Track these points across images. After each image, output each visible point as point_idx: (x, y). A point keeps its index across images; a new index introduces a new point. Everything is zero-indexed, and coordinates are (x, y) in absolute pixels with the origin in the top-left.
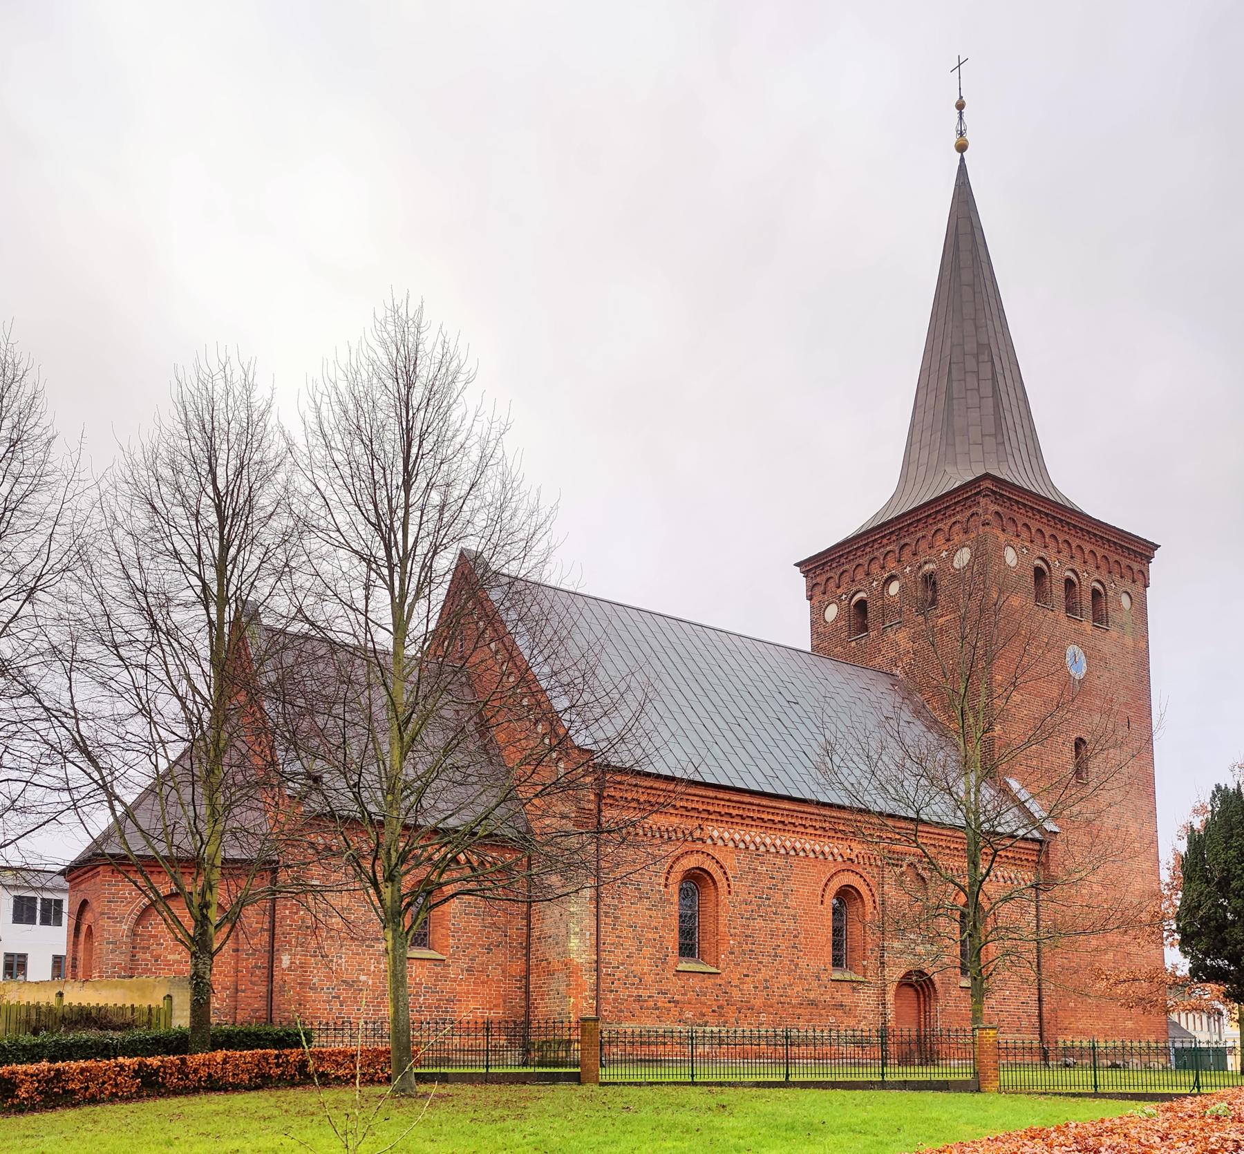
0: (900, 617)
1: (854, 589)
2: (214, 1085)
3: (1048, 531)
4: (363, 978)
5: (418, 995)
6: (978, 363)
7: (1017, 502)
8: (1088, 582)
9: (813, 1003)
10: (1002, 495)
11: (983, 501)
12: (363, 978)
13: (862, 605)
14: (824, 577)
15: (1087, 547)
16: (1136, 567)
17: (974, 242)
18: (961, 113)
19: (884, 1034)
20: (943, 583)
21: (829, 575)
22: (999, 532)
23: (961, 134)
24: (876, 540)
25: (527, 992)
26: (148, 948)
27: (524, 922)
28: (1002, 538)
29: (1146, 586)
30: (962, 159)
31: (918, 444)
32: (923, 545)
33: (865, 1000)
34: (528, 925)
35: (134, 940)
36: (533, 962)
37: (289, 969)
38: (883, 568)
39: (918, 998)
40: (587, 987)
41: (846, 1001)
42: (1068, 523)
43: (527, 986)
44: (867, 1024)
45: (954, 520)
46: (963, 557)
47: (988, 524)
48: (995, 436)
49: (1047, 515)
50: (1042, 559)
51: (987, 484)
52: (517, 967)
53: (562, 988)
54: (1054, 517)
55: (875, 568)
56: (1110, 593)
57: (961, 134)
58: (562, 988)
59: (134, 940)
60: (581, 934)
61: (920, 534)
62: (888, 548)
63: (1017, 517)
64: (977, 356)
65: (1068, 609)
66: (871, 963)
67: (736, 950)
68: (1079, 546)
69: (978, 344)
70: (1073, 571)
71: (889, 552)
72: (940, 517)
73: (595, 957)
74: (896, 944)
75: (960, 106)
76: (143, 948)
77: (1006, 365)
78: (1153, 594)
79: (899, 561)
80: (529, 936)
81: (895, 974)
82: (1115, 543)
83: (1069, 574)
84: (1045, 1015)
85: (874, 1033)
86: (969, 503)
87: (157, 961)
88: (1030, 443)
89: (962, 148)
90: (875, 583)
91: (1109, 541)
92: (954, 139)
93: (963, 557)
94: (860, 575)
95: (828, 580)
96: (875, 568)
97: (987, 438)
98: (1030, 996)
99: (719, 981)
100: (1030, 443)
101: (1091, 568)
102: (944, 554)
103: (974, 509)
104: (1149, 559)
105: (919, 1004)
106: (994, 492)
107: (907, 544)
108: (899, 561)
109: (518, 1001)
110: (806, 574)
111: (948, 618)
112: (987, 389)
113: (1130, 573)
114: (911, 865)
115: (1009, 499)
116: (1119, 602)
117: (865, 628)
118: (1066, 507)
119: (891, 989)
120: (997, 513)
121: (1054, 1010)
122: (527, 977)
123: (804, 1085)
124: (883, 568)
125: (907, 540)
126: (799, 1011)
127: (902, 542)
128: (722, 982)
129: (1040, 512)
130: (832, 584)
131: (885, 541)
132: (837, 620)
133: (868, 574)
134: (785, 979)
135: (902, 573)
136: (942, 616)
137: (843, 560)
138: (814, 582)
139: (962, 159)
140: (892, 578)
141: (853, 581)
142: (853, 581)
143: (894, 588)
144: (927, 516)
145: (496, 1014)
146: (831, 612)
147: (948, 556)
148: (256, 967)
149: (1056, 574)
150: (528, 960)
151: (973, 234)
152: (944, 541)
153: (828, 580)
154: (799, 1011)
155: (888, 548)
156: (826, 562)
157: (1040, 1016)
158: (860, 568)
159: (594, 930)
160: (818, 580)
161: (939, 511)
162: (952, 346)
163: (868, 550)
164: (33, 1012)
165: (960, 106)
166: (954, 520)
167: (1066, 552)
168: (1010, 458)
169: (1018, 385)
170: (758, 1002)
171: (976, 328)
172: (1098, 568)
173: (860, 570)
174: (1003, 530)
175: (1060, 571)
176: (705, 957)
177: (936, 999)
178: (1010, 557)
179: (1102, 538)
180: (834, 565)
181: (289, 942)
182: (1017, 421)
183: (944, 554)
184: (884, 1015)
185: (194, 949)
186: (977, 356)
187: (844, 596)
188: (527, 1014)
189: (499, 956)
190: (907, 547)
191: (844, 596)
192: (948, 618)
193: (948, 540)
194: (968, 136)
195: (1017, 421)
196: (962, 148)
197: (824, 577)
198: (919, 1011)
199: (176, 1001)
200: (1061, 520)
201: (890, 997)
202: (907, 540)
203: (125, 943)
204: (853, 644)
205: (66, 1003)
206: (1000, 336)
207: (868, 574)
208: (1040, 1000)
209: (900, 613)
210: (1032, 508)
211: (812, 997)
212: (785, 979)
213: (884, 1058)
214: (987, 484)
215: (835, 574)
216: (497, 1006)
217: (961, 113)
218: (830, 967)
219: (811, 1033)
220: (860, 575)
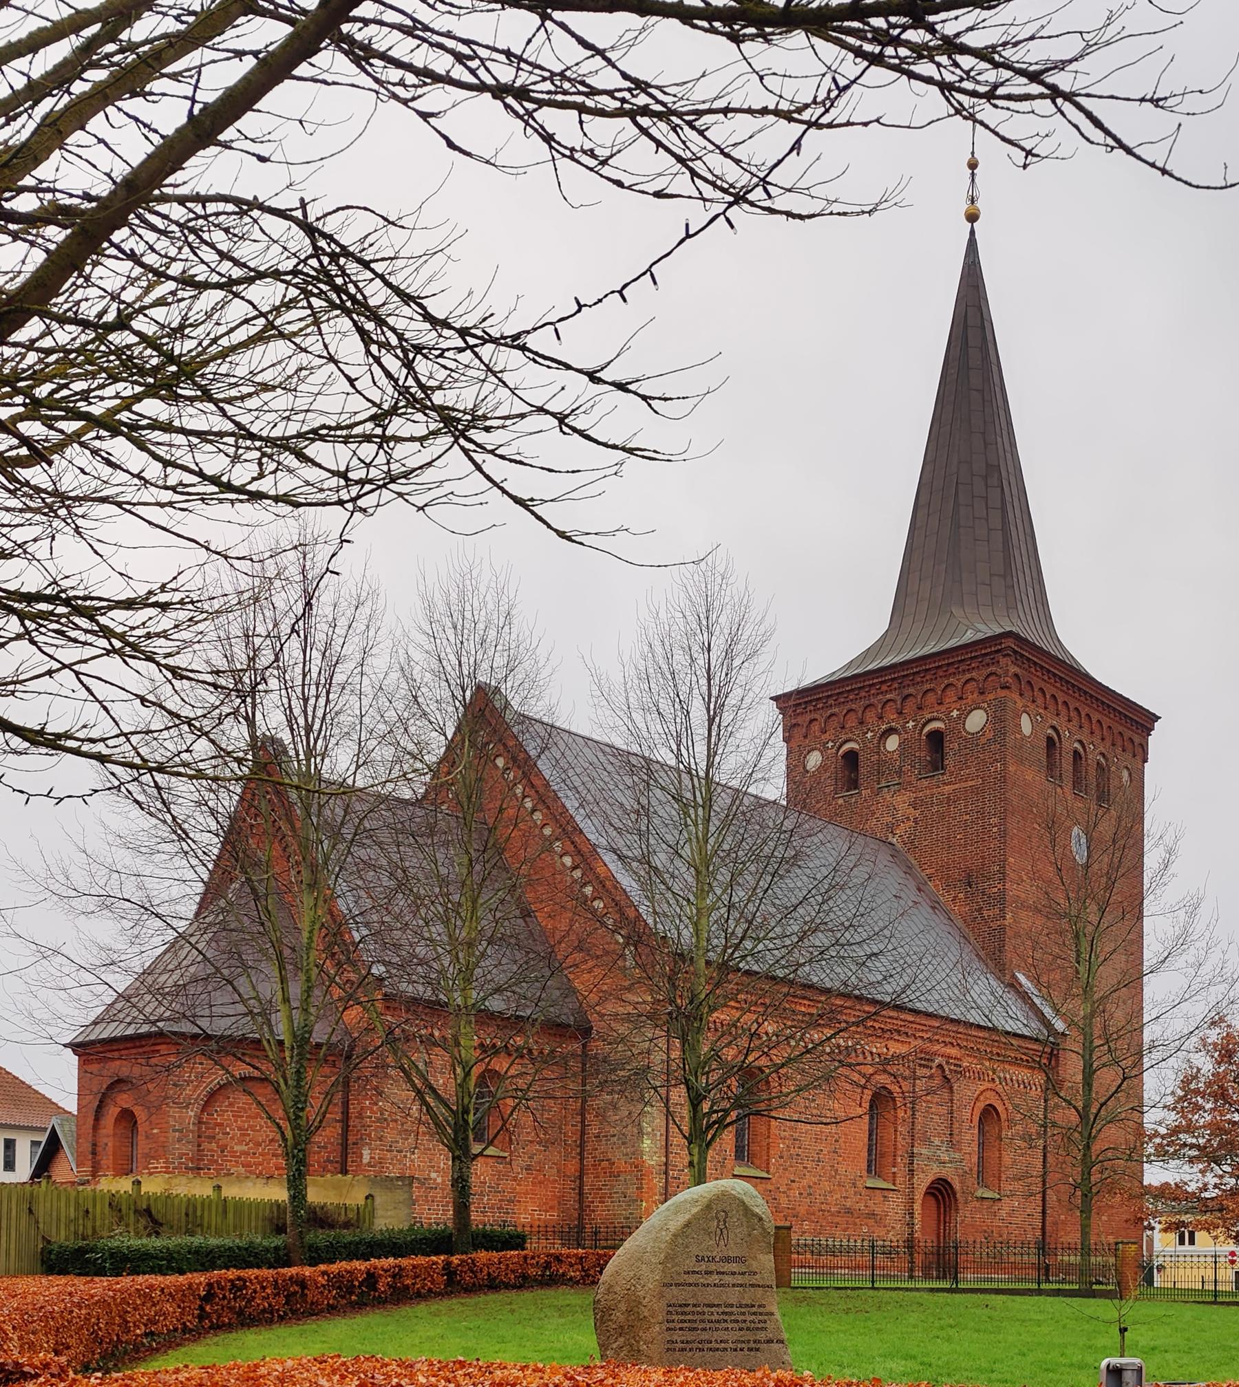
0: (900, 777)
1: (844, 737)
2: (493, 1285)
3: (1061, 698)
4: (433, 1175)
5: (482, 1194)
6: (986, 485)
7: (1035, 663)
8: (1093, 756)
9: (849, 1211)
10: (1022, 656)
11: (1003, 661)
12: (433, 1175)
13: (852, 757)
14: (808, 717)
15: (1095, 717)
16: (1137, 739)
17: (984, 338)
18: (973, 174)
19: (910, 1244)
20: (951, 746)
21: (813, 716)
22: (1016, 696)
23: (973, 202)
24: (873, 684)
25: (581, 1194)
26: (214, 1137)
27: (579, 1118)
28: (1020, 704)
29: (1145, 760)
30: (972, 232)
31: (918, 574)
32: (931, 698)
33: (894, 1207)
34: (583, 1122)
35: (199, 1129)
36: (589, 1161)
37: (369, 1164)
38: (881, 718)
39: (939, 1208)
40: (657, 1191)
41: (878, 1210)
42: (1080, 689)
43: (581, 1188)
44: (894, 1235)
45: (968, 676)
46: (976, 721)
47: (1008, 688)
48: (1004, 577)
49: (1061, 678)
50: (1054, 728)
51: (1010, 643)
52: (572, 1167)
53: (631, 1191)
54: (1067, 682)
55: (871, 716)
56: (1113, 769)
57: (973, 202)
58: (631, 1191)
59: (199, 1129)
60: (652, 1135)
61: (927, 686)
62: (888, 696)
63: (1034, 680)
64: (986, 478)
65: (1099, 799)
66: (901, 1170)
67: (785, 1154)
68: (1099, 721)
69: (987, 465)
70: (1080, 742)
71: (889, 701)
72: (952, 670)
73: (664, 1159)
74: (924, 1151)
75: (973, 165)
76: (209, 1137)
77: (1015, 491)
78: (1151, 771)
79: (901, 713)
80: (583, 1133)
81: (923, 1182)
82: (1120, 713)
83: (1076, 745)
84: (1048, 1228)
85: (901, 1243)
86: (987, 660)
87: (222, 1151)
88: (1037, 587)
89: (972, 217)
90: (869, 735)
91: (1114, 709)
92: (964, 206)
93: (976, 721)
94: (852, 722)
95: (811, 721)
96: (871, 716)
97: (996, 578)
98: (1035, 1207)
99: (770, 1187)
100: (1037, 587)
101: (1097, 740)
102: (955, 713)
103: (993, 669)
104: (1149, 730)
105: (939, 1214)
106: (1015, 652)
107: (910, 695)
108: (901, 713)
109: (572, 1203)
110: (782, 710)
111: (956, 786)
112: (996, 521)
113: (1131, 746)
114: (940, 1066)
115: (1028, 659)
116: (1121, 778)
117: (854, 784)
118: (1072, 666)
119: (919, 1196)
120: (1016, 675)
121: (1056, 1223)
122: (581, 1178)
123: (1222, 1303)
124: (881, 718)
125: (911, 690)
126: (837, 1220)
127: (906, 692)
128: (771, 1188)
129: (1055, 675)
130: (815, 727)
131: (884, 688)
132: (822, 768)
133: (861, 723)
134: (826, 1185)
135: (904, 727)
136: (950, 784)
137: (831, 702)
138: (794, 721)
139: (972, 232)
140: (891, 731)
141: (843, 728)
142: (843, 728)
143: (892, 743)
144: (937, 668)
145: (552, 1216)
146: (814, 760)
147: (959, 717)
148: (328, 1161)
149: (1065, 744)
150: (582, 1160)
151: (984, 328)
152: (955, 699)
153: (811, 721)
154: (837, 1220)
155: (888, 696)
156: (811, 701)
157: (1043, 1229)
158: (851, 714)
159: (663, 1130)
160: (800, 720)
161: (952, 663)
162: (960, 462)
163: (863, 694)
164: (275, 1209)
165: (973, 165)
166: (968, 676)
167: (1040, 701)
168: (1019, 606)
169: (1026, 517)
170: (802, 1210)
171: (986, 445)
172: (1103, 739)
173: (852, 715)
174: (1021, 695)
175: (1069, 744)
176: (755, 1161)
177: (957, 1210)
178: (1026, 725)
179: (1109, 706)
180: (820, 706)
181: (369, 1135)
182: (1025, 560)
183: (955, 713)
184: (911, 1225)
185: (457, 1153)
186: (986, 478)
187: (830, 744)
188: (580, 1218)
189: (555, 1154)
190: (911, 698)
191: (830, 744)
192: (956, 786)
193: (961, 698)
194: (979, 204)
195: (1025, 560)
196: (972, 217)
197: (808, 717)
198: (939, 1221)
199: (378, 1200)
200: (1073, 686)
201: (917, 1207)
202: (911, 690)
203: (192, 1132)
204: (841, 801)
205: (143, 1190)
206: (1009, 455)
207: (861, 723)
208: (1044, 1212)
209: (900, 773)
210: (1049, 671)
211: (848, 1204)
212: (826, 1185)
213: (911, 1270)
214: (1010, 643)
215: (820, 716)
216: (551, 1208)
217: (973, 174)
218: (865, 1173)
219: (845, 1243)
220: (852, 722)
